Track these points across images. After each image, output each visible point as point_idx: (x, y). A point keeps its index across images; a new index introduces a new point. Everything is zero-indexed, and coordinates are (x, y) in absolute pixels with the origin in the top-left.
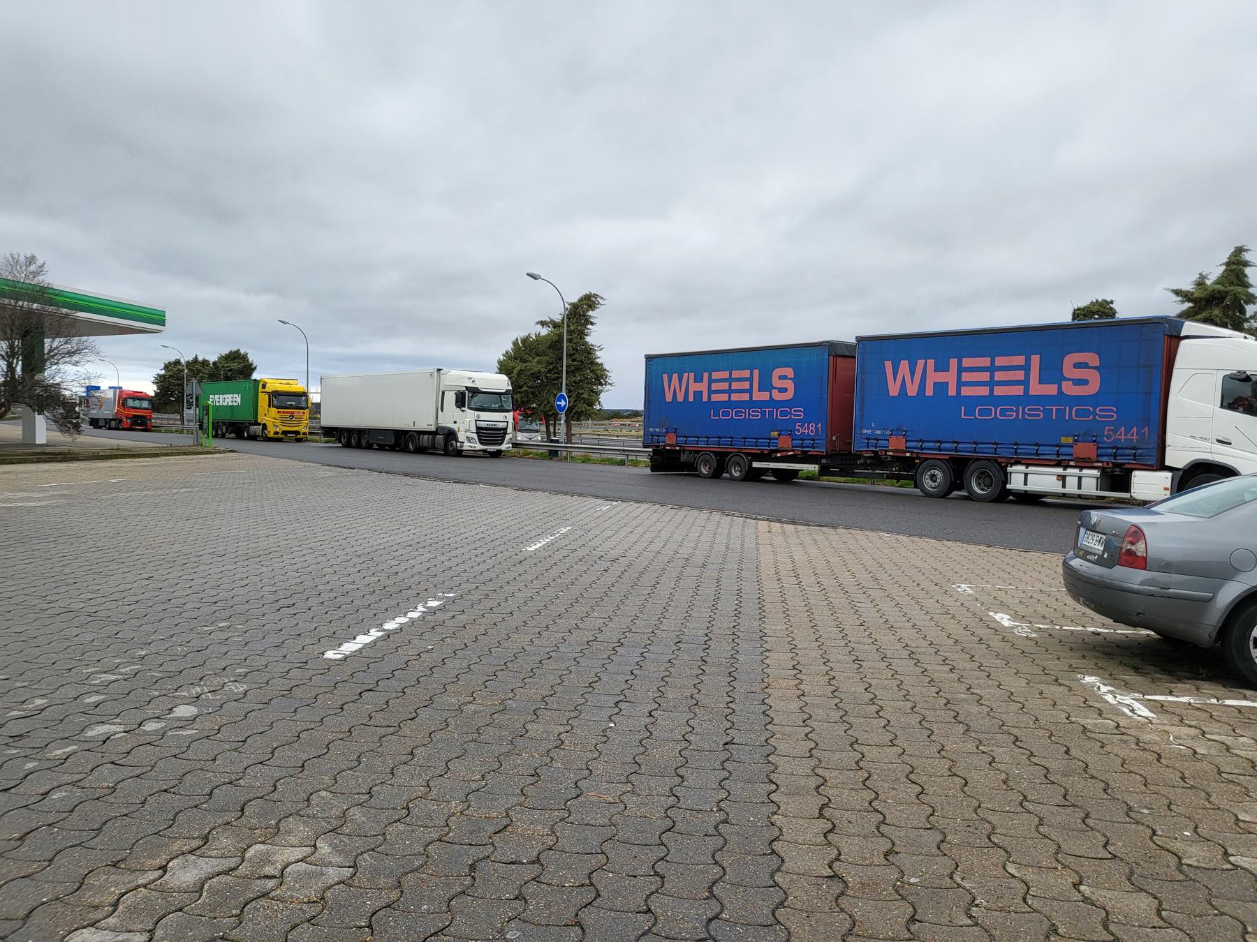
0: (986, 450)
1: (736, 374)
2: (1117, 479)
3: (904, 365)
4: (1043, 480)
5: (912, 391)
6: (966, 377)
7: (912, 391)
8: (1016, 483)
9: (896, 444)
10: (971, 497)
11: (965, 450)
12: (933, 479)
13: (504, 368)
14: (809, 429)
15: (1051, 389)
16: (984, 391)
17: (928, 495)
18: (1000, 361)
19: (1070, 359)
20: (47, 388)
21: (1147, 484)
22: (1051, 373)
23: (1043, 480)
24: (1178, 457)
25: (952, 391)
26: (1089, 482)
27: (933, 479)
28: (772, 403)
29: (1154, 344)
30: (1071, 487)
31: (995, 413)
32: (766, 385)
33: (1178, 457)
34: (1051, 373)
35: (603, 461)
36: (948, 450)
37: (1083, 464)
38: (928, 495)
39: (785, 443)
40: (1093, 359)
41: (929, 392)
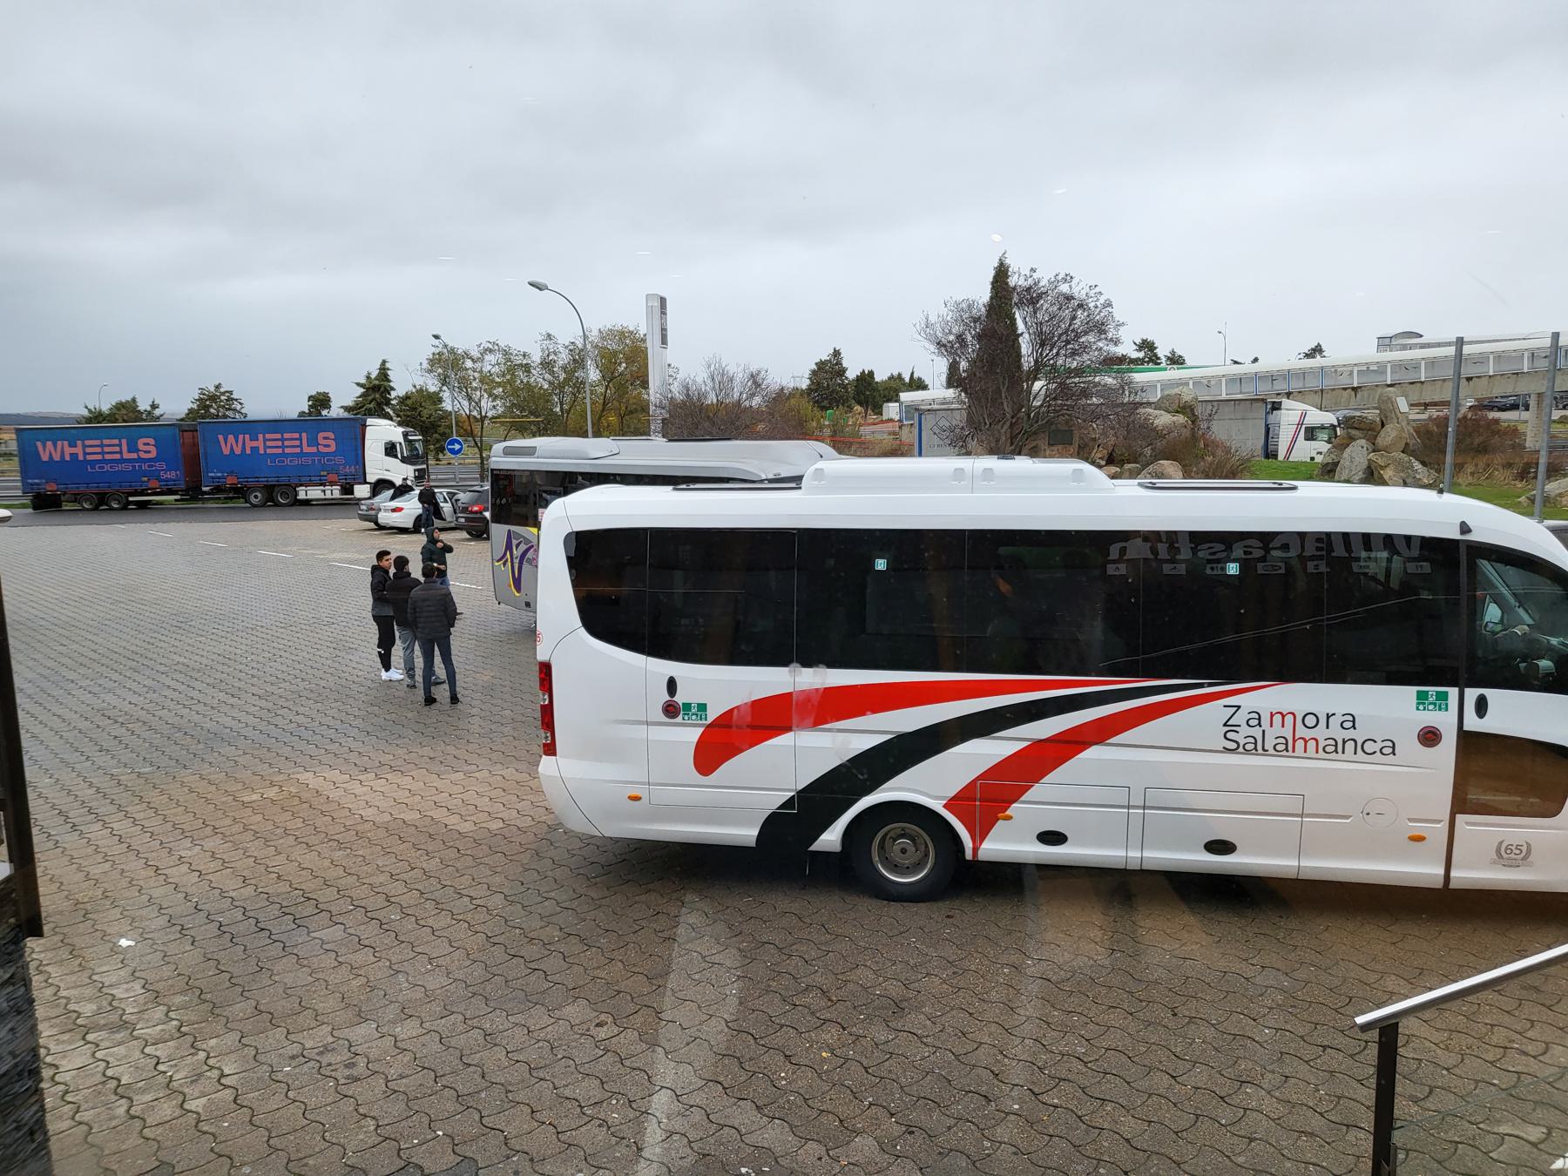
0: (284, 480)
1: (106, 442)
2: (347, 489)
3: (231, 437)
4: (314, 493)
5: (238, 451)
6: (88, 450)
7: (238, 451)
8: (302, 496)
9: (231, 480)
10: (112, 509)
11: (272, 481)
12: (257, 497)
13: (949, 385)
14: (171, 475)
15: (314, 449)
16: (99, 457)
17: (254, 506)
18: (286, 436)
19: (321, 435)
20: (989, 311)
21: (361, 491)
22: (313, 441)
23: (314, 493)
24: (371, 478)
25: (81, 458)
26: (335, 492)
27: (257, 497)
28: (140, 460)
29: (352, 431)
30: (328, 495)
31: (107, 468)
32: (133, 448)
33: (371, 478)
34: (313, 441)
35: (762, 481)
36: (93, 488)
37: (332, 484)
38: (254, 506)
39: (154, 484)
40: (331, 435)
41: (67, 458)
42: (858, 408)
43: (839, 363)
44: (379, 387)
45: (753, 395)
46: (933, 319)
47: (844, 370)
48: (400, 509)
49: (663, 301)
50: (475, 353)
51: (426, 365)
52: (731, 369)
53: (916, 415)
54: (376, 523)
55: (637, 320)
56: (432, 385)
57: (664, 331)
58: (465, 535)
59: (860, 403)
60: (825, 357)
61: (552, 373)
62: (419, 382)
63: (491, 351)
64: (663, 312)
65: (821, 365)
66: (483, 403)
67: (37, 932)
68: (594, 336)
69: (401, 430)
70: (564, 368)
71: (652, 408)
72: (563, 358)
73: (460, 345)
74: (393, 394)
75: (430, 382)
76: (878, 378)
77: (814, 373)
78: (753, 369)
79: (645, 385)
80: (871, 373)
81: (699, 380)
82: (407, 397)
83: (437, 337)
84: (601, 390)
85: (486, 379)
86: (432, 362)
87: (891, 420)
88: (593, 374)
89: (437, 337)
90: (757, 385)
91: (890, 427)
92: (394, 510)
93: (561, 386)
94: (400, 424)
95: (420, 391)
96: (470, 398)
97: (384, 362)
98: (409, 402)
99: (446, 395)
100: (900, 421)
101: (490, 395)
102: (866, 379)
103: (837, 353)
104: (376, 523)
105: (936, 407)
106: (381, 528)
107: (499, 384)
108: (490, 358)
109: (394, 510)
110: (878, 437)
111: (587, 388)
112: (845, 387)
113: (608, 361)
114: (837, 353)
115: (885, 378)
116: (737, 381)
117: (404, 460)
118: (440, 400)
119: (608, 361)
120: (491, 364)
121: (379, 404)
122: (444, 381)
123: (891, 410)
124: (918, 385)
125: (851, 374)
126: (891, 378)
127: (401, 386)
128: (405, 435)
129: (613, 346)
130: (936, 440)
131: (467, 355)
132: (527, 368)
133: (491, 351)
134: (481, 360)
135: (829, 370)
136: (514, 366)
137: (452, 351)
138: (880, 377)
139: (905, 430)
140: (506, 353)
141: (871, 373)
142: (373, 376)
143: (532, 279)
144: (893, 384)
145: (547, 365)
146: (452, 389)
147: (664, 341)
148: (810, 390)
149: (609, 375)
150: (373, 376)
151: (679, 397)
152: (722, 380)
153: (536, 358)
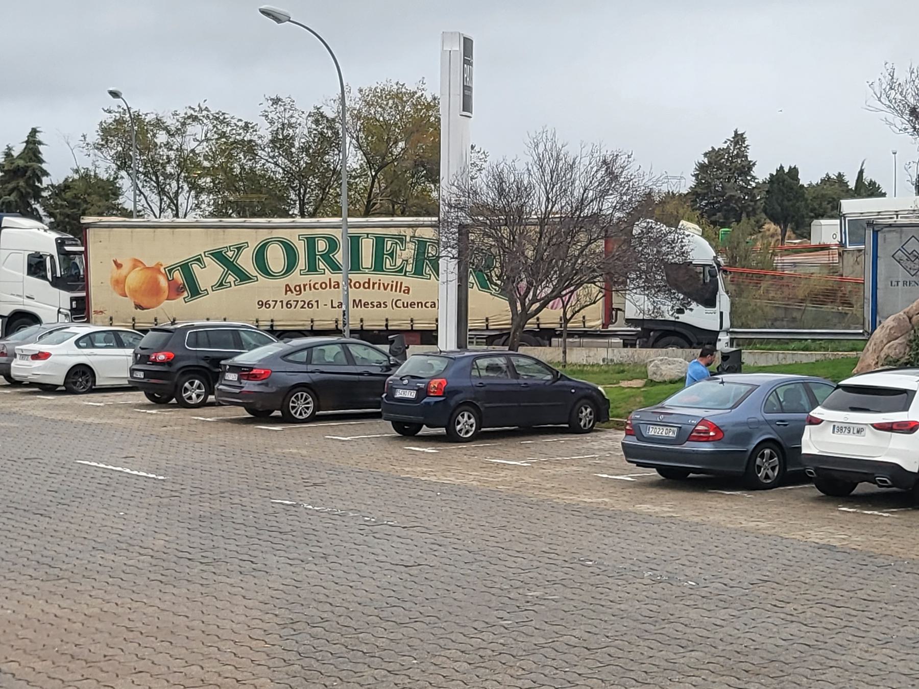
42: (771, 227)
43: (742, 155)
44: (25, 169)
45: (604, 194)
46: (902, 76)
47: (750, 166)
48: (45, 356)
49: (468, 44)
50: (172, 123)
51: (94, 137)
52: (572, 151)
53: (869, 233)
54: (8, 377)
55: (421, 71)
56: (103, 167)
57: (467, 88)
58: (140, 397)
59: (776, 221)
60: (720, 145)
61: (289, 155)
62: (85, 163)
63: (195, 119)
64: (467, 61)
65: (714, 156)
66: (181, 199)
67: (627, 434)
68: (354, 101)
69: (54, 235)
70: (305, 149)
71: (443, 209)
72: (303, 132)
73: (147, 106)
74: (46, 181)
75: (103, 165)
76: (804, 180)
77: (702, 168)
78: (607, 151)
79: (434, 176)
80: (794, 172)
81: (521, 167)
82: (66, 186)
83: (115, 94)
84: (362, 183)
85: (187, 163)
86: (107, 132)
87: (824, 248)
88: (354, 159)
89: (115, 94)
90: (613, 177)
91: (822, 258)
92: (36, 356)
93: (302, 175)
94: (52, 227)
95: (85, 177)
96: (161, 192)
97: (34, 131)
98: (69, 195)
99: (125, 182)
100: (842, 244)
101: (193, 186)
102: (785, 180)
103: (739, 139)
104: (8, 377)
105: (900, 221)
106: (15, 383)
107: (207, 172)
108: (195, 130)
109: (36, 356)
110: (800, 271)
111: (344, 180)
112: (750, 193)
113: (376, 138)
114: (739, 139)
115: (816, 181)
116: (580, 168)
117: (56, 283)
118: (116, 192)
119: (376, 138)
120: (196, 140)
121: (23, 197)
122: (123, 162)
123: (826, 231)
124: (867, 189)
125: (762, 173)
126: (827, 180)
127: (58, 167)
128: (60, 244)
129: (387, 115)
130: (901, 274)
131: (158, 124)
132: (250, 148)
133: (195, 119)
134: (180, 131)
135: (725, 167)
136: (234, 143)
137: (137, 119)
138: (808, 178)
139: (849, 259)
140: (220, 119)
141: (794, 172)
142: (15, 153)
143: (263, 7)
144: (829, 191)
145: (281, 143)
146: (134, 177)
147: (467, 106)
148: (694, 194)
149: (377, 159)
150: (15, 153)
151: (489, 196)
152: (558, 173)
153: (264, 132)
